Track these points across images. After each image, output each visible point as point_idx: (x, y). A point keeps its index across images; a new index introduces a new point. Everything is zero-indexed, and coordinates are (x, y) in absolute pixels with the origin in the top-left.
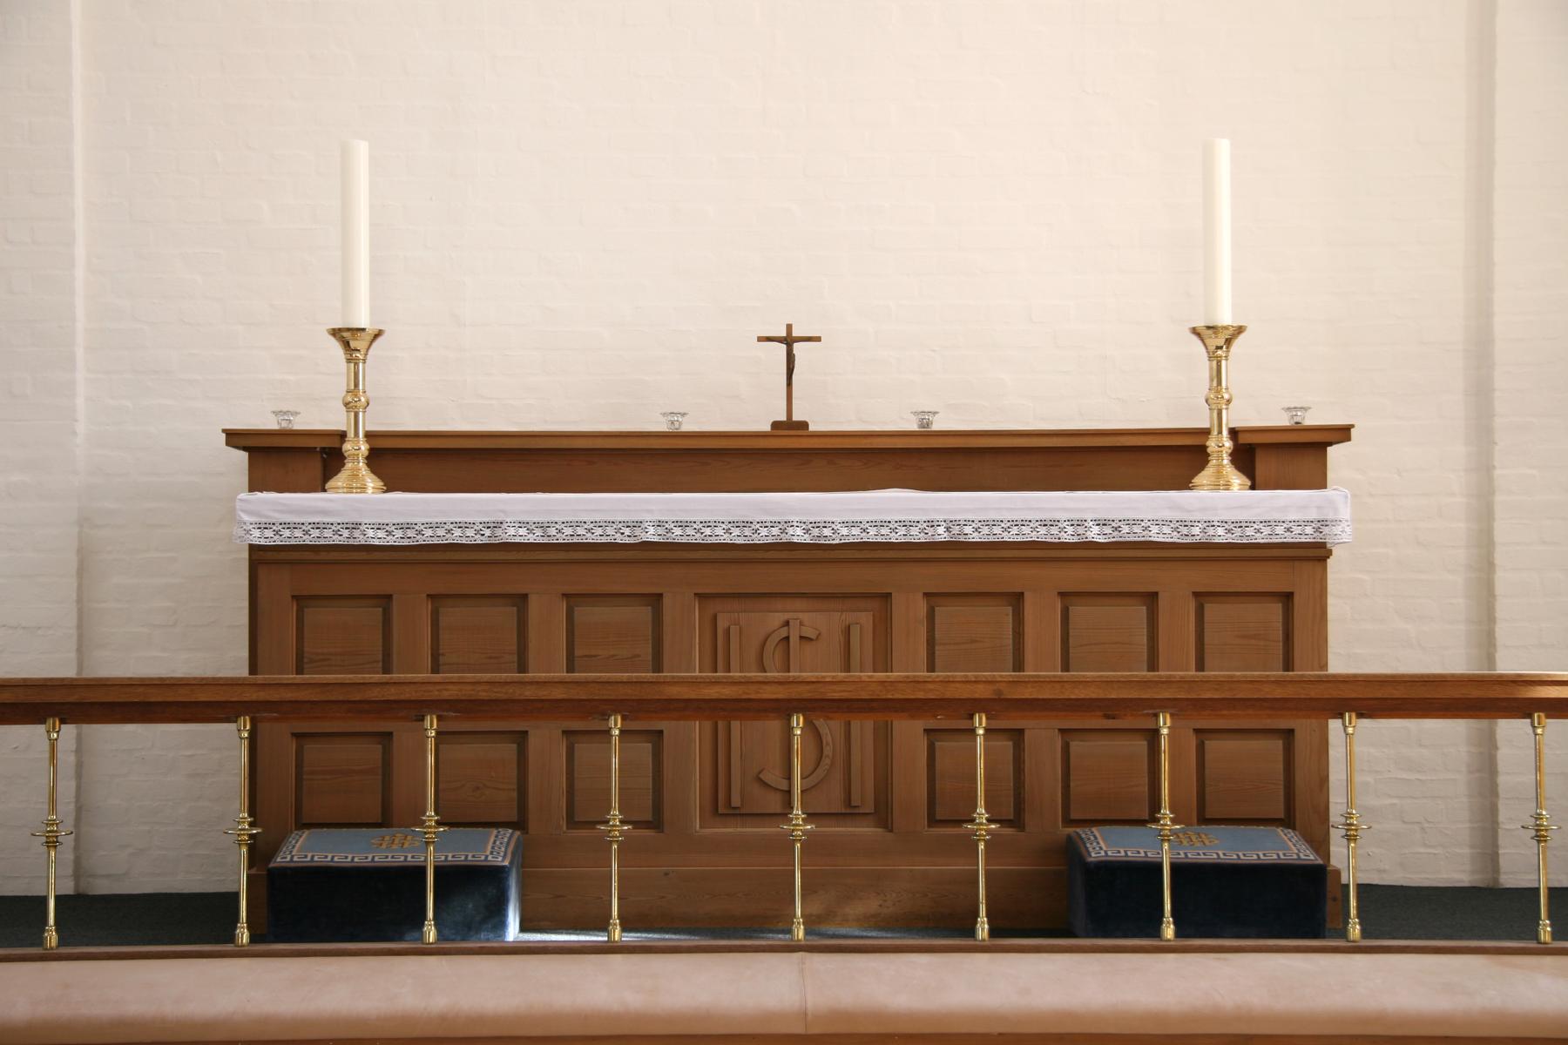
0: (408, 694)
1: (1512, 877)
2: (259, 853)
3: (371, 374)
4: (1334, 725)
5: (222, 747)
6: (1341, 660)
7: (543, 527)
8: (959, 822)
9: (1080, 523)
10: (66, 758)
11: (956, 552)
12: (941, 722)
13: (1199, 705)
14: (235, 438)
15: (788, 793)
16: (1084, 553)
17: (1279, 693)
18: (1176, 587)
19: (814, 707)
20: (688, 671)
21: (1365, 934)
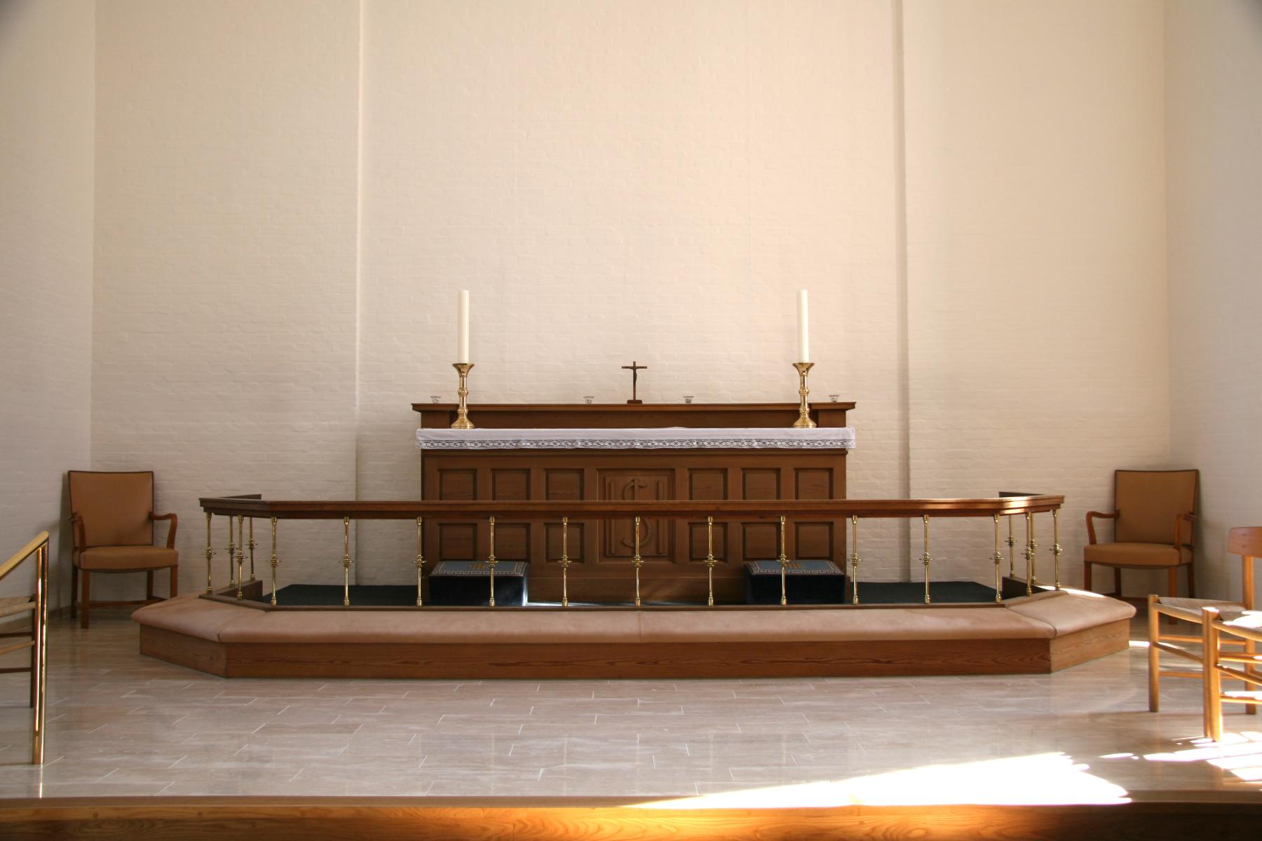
0: (483, 508)
1: (915, 579)
2: (426, 570)
3: (469, 382)
4: (849, 520)
5: (412, 528)
6: (850, 496)
7: (537, 442)
8: (702, 559)
9: (750, 441)
10: (246, 531)
11: (700, 452)
12: (747, 520)
13: (797, 513)
14: (416, 407)
15: (634, 548)
16: (752, 452)
17: (827, 508)
18: (788, 467)
19: (645, 514)
20: (594, 499)
21: (860, 602)
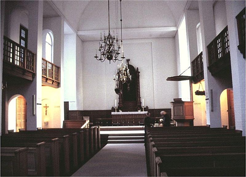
18: (142, 115)
